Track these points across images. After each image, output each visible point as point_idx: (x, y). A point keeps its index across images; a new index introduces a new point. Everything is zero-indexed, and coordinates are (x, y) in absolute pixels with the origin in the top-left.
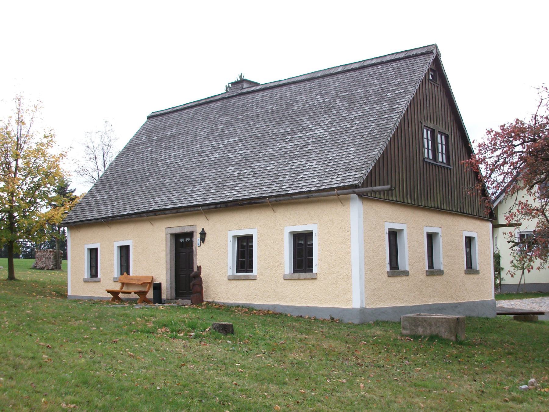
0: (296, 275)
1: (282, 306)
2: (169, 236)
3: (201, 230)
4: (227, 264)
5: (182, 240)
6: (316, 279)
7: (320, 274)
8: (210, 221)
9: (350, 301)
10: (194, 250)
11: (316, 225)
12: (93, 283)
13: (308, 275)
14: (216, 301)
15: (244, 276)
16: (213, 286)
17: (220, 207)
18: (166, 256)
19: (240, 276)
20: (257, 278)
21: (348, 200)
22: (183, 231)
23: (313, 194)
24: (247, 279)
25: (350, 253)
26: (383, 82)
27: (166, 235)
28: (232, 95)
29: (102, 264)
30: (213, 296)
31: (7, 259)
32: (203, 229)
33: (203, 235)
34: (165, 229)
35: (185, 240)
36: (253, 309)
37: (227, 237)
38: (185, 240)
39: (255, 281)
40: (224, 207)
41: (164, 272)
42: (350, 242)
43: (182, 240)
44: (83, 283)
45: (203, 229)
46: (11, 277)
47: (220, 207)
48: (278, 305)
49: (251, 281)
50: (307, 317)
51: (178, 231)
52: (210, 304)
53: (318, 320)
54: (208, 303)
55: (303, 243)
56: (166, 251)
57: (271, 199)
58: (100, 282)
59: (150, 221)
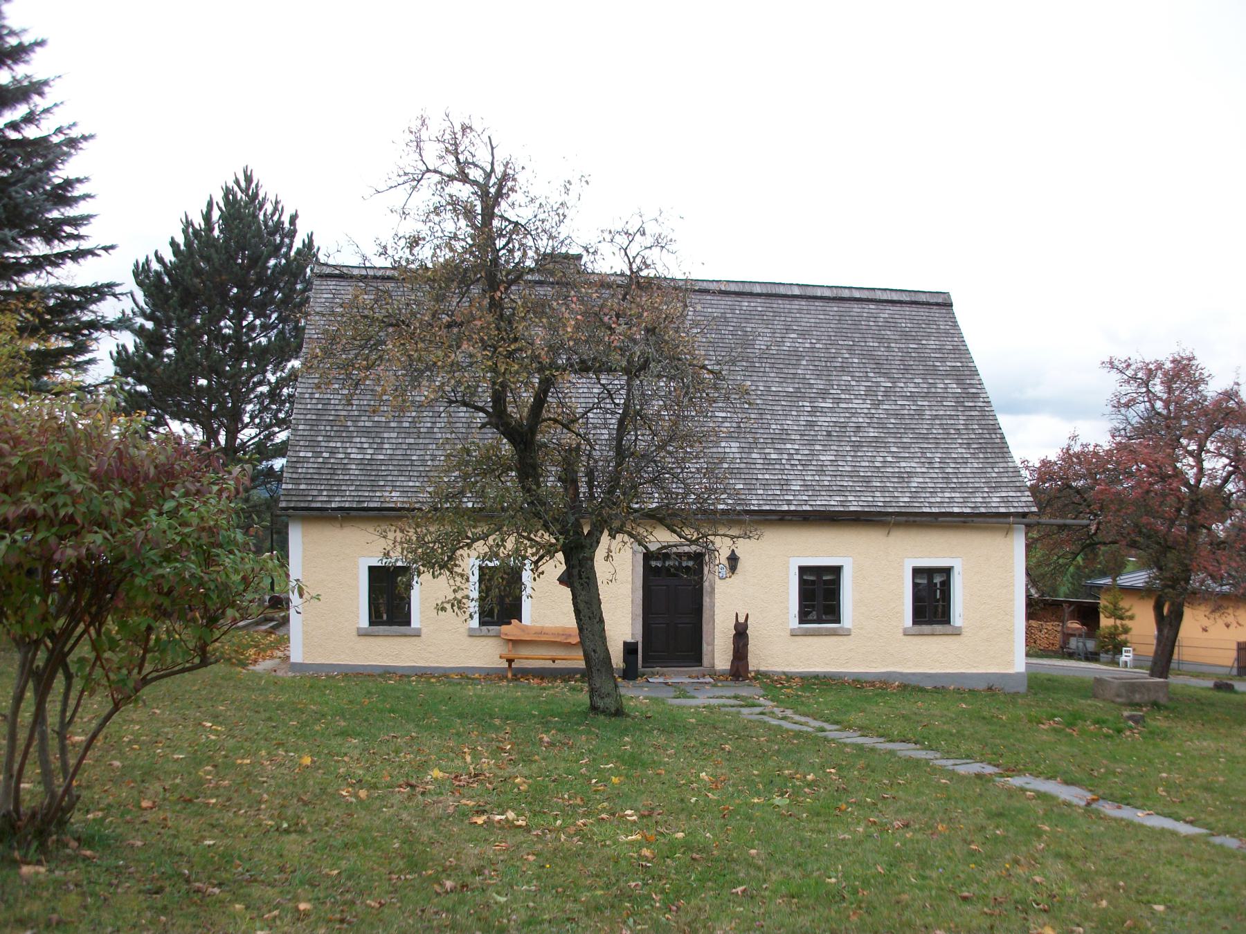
0: (917, 628)
3: (729, 553)
5: (653, 564)
9: (1011, 663)
10: (706, 584)
17: (791, 520)
18: (633, 591)
24: (834, 633)
25: (1012, 600)
31: (297, 537)
33: (733, 560)
43: (653, 564)
52: (760, 675)
54: (758, 672)
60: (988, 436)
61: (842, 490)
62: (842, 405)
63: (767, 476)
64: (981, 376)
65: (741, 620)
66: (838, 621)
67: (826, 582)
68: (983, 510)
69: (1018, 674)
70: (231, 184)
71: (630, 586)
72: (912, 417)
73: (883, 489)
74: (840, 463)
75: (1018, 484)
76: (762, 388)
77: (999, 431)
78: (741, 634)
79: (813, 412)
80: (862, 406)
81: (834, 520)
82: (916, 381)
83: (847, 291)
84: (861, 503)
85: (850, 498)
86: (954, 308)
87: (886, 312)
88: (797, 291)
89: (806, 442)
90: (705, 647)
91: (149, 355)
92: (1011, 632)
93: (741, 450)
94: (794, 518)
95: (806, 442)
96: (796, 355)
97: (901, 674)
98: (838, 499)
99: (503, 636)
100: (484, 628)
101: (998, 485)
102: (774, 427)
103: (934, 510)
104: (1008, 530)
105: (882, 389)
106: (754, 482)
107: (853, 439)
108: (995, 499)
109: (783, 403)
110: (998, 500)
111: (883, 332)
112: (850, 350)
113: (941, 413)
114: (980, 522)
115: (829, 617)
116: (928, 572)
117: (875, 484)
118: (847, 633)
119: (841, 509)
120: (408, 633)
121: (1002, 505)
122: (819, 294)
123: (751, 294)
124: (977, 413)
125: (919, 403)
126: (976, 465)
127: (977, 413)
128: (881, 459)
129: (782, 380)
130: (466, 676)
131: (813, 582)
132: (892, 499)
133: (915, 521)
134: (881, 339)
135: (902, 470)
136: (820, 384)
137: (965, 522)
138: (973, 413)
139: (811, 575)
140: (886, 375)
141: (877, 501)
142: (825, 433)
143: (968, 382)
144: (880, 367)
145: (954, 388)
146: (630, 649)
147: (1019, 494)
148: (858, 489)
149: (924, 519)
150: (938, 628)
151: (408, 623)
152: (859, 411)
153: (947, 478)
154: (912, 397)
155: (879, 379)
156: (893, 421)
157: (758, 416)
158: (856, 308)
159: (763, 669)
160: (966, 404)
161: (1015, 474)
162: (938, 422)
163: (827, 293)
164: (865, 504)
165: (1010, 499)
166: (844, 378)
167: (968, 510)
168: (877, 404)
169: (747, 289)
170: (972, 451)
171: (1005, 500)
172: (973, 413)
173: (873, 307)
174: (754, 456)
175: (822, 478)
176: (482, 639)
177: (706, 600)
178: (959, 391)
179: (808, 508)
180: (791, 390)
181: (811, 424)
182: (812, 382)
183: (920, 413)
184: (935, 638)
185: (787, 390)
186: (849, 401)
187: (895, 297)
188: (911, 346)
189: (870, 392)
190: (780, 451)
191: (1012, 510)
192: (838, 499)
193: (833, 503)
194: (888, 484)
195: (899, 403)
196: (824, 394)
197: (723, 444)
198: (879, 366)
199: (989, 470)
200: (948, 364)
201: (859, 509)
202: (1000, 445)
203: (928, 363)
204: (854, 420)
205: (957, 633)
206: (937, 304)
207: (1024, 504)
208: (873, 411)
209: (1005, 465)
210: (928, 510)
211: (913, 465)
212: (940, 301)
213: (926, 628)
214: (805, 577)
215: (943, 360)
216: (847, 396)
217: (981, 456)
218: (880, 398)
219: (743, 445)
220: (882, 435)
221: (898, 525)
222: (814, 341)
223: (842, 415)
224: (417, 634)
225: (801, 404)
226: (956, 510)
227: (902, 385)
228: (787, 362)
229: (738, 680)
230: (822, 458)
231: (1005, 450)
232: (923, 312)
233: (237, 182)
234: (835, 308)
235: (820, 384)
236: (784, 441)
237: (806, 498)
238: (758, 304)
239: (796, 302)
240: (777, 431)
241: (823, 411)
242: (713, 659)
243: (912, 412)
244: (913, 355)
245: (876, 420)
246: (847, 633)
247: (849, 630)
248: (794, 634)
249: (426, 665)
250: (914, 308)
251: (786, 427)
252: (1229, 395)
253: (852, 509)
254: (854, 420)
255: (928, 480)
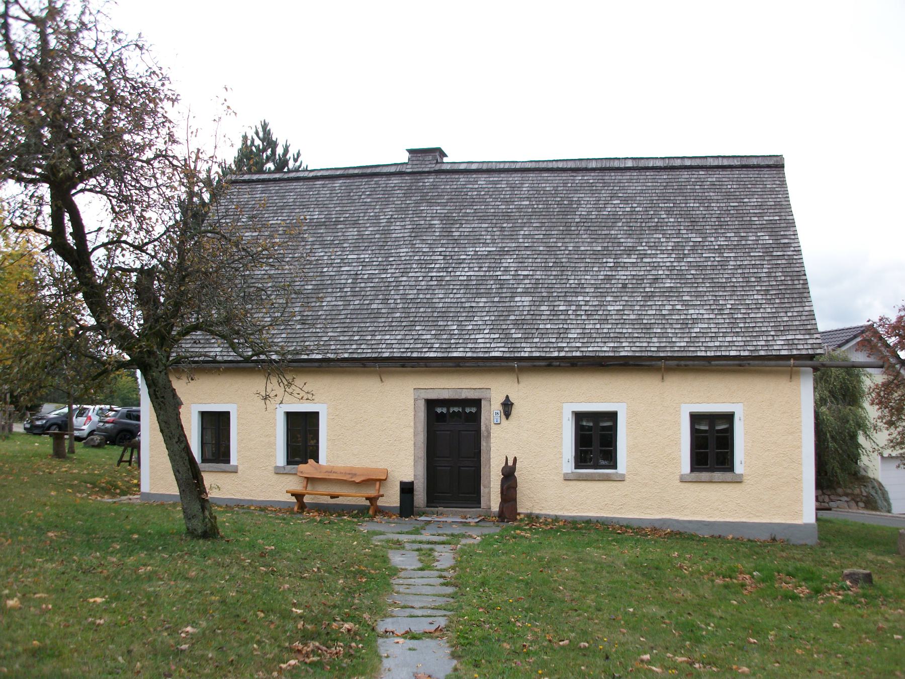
2: (422, 405)
4: (561, 454)
5: (439, 410)
6: (740, 482)
7: (748, 475)
8: (522, 385)
10: (483, 428)
11: (742, 404)
13: (728, 476)
15: (586, 474)
16: (529, 489)
17: (559, 366)
18: (415, 435)
19: (603, 474)
20: (626, 479)
21: (798, 373)
22: (457, 397)
23: (751, 362)
24: (607, 478)
26: (604, 221)
27: (415, 400)
29: (240, 442)
30: (529, 505)
32: (507, 397)
33: (507, 407)
34: (412, 391)
35: (448, 410)
37: (562, 413)
38: (448, 410)
39: (232, 475)
40: (568, 367)
41: (411, 462)
42: (801, 432)
43: (439, 410)
44: (677, 483)
45: (507, 397)
47: (559, 366)
48: (670, 519)
52: (532, 518)
55: (706, 428)
58: (236, 472)
59: (381, 375)
60: (790, 282)
61: (619, 337)
63: (548, 326)
64: (798, 228)
65: (510, 463)
66: (615, 467)
67: (604, 428)
68: (762, 353)
69: (806, 525)
71: (412, 430)
72: (714, 268)
73: (661, 336)
74: (626, 312)
75: (809, 327)
76: (570, 248)
77: (804, 277)
78: (509, 475)
79: (615, 267)
80: (665, 260)
81: (603, 366)
82: (728, 235)
83: (679, 160)
84: (633, 349)
85: (624, 344)
86: (785, 169)
87: (713, 177)
88: (629, 164)
90: (483, 490)
92: (798, 481)
93: (532, 303)
94: (562, 364)
95: (598, 294)
96: (615, 218)
97: (677, 521)
98: (612, 345)
99: (299, 474)
100: (290, 466)
101: (786, 328)
102: (571, 282)
103: (709, 354)
104: (792, 374)
105: (691, 244)
106: (534, 331)
107: (647, 290)
108: (779, 342)
109: (588, 260)
110: (782, 343)
112: (669, 212)
113: (746, 263)
114: (758, 366)
116: (712, 418)
117: (655, 331)
118: (621, 479)
119: (611, 354)
120: (227, 469)
121: (786, 347)
123: (586, 170)
124: (784, 262)
125: (725, 255)
126: (769, 310)
127: (784, 262)
128: (670, 307)
129: (593, 240)
130: (263, 508)
131: (590, 429)
132: (667, 344)
133: (686, 365)
134: (701, 200)
135: (689, 317)
136: (630, 242)
137: (740, 365)
138: (779, 262)
139: (607, 421)
140: (699, 232)
141: (653, 346)
143: (782, 233)
144: (693, 224)
145: (767, 239)
146: (407, 489)
147: (807, 337)
148: (636, 335)
149: (696, 363)
150: (717, 475)
152: (661, 264)
153: (734, 323)
154: (720, 250)
156: (693, 272)
157: (559, 273)
159: (536, 511)
160: (775, 254)
161: (809, 317)
162: (740, 271)
165: (796, 342)
166: (655, 236)
167: (746, 353)
168: (679, 259)
170: (769, 297)
171: (790, 344)
172: (779, 262)
174: (543, 308)
175: (603, 326)
176: (286, 476)
177: (483, 443)
178: (771, 242)
179: (578, 354)
180: (599, 248)
181: (608, 278)
182: (622, 240)
183: (723, 265)
186: (651, 256)
187: (726, 162)
188: (732, 204)
190: (570, 304)
191: (795, 352)
192: (612, 345)
193: (605, 349)
194: (669, 331)
195: (704, 255)
196: (629, 251)
197: (517, 299)
198: (694, 224)
199: (782, 314)
200: (766, 218)
202: (801, 291)
204: (653, 272)
205: (739, 481)
206: (768, 166)
207: (809, 347)
208: (675, 264)
209: (801, 309)
210: (703, 354)
212: (771, 163)
213: (705, 475)
215: (760, 215)
216: (653, 252)
217: (777, 301)
218: (686, 252)
219: (536, 299)
220: (679, 285)
222: (635, 205)
223: (643, 269)
224: (235, 471)
225: (605, 260)
226: (733, 353)
227: (713, 239)
228: (603, 224)
230: (609, 308)
231: (805, 295)
232: (752, 174)
233: (257, 133)
234: (664, 175)
235: (630, 242)
236: (577, 294)
237: (580, 345)
238: (590, 178)
239: (628, 174)
240: (573, 286)
241: (625, 267)
242: (490, 501)
243: (716, 263)
244: (732, 212)
245: (676, 272)
246: (621, 479)
247: (624, 475)
248: (567, 478)
249: (242, 498)
250: (744, 171)
251: (583, 281)
253: (622, 354)
254: (653, 272)
255: (712, 326)
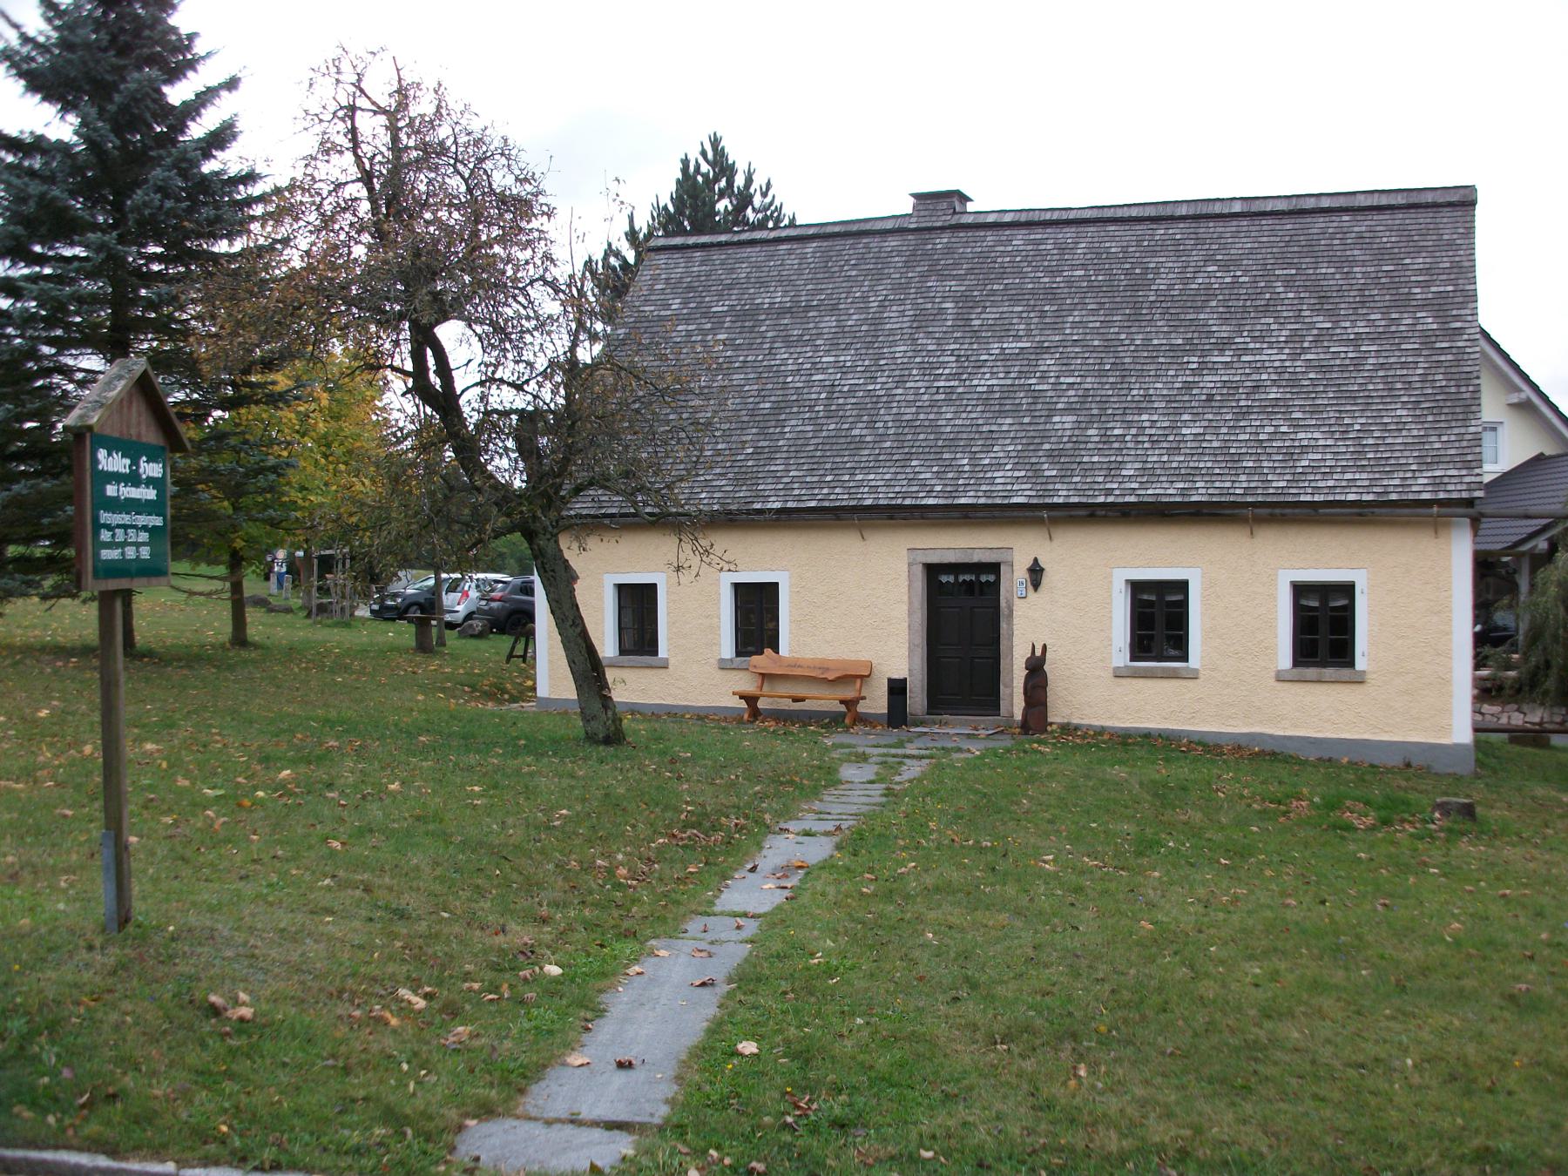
1: (1271, 736)
3: (1029, 563)
4: (1111, 640)
8: (1056, 542)
12: (637, 670)
13: (1345, 673)
14: (1075, 721)
17: (1105, 516)
18: (910, 613)
21: (1448, 525)
23: (1376, 510)
27: (910, 565)
28: (930, 225)
32: (1036, 560)
36: (1129, 736)
42: (1451, 611)
43: (944, 579)
45: (1036, 560)
46: (239, 638)
47: (1105, 516)
49: (1184, 683)
50: (1345, 760)
51: (934, 558)
53: (1462, 777)
56: (910, 603)
57: (1258, 511)
61: (1193, 473)
62: (1244, 358)
66: (1185, 658)
70: (694, 155)
71: (905, 607)
81: (1167, 516)
88: (1237, 208)
89: (1172, 411)
91: (153, 315)
92: (1445, 682)
93: (1076, 425)
94: (1110, 514)
95: (1172, 411)
101: (1436, 459)
111: (1348, 253)
115: (1173, 652)
118: (1193, 676)
122: (1269, 209)
123: (1172, 218)
130: (703, 716)
131: (1150, 604)
133: (1283, 515)
136: (1224, 331)
137: (1360, 515)
141: (1239, 487)
142: (1204, 397)
143: (1454, 312)
148: (1217, 471)
149: (1297, 511)
151: (655, 653)
152: (1267, 364)
154: (1357, 340)
155: (1315, 319)
158: (1320, 222)
163: (1282, 206)
164: (1217, 492)
166: (1263, 321)
168: (1294, 356)
169: (1168, 211)
171: (1437, 483)
173: (1347, 218)
176: (735, 673)
177: (1003, 625)
179: (1132, 499)
181: (1188, 386)
184: (1324, 687)
185: (1174, 342)
187: (1384, 201)
189: (1295, 337)
201: (1204, 499)
203: (1401, 291)
211: (1316, 435)
213: (1311, 672)
214: (1304, 602)
215: (1425, 285)
219: (1082, 419)
220: (1289, 396)
221: (1261, 521)
224: (664, 666)
225: (1185, 360)
229: (1026, 734)
232: (1424, 217)
234: (1289, 225)
246: (1193, 676)
247: (1196, 671)
248: (1119, 674)
249: (675, 703)
250: (1412, 214)
252: (185, 76)
253: (1194, 499)
